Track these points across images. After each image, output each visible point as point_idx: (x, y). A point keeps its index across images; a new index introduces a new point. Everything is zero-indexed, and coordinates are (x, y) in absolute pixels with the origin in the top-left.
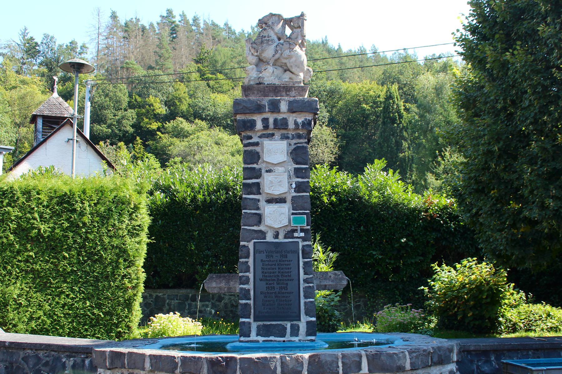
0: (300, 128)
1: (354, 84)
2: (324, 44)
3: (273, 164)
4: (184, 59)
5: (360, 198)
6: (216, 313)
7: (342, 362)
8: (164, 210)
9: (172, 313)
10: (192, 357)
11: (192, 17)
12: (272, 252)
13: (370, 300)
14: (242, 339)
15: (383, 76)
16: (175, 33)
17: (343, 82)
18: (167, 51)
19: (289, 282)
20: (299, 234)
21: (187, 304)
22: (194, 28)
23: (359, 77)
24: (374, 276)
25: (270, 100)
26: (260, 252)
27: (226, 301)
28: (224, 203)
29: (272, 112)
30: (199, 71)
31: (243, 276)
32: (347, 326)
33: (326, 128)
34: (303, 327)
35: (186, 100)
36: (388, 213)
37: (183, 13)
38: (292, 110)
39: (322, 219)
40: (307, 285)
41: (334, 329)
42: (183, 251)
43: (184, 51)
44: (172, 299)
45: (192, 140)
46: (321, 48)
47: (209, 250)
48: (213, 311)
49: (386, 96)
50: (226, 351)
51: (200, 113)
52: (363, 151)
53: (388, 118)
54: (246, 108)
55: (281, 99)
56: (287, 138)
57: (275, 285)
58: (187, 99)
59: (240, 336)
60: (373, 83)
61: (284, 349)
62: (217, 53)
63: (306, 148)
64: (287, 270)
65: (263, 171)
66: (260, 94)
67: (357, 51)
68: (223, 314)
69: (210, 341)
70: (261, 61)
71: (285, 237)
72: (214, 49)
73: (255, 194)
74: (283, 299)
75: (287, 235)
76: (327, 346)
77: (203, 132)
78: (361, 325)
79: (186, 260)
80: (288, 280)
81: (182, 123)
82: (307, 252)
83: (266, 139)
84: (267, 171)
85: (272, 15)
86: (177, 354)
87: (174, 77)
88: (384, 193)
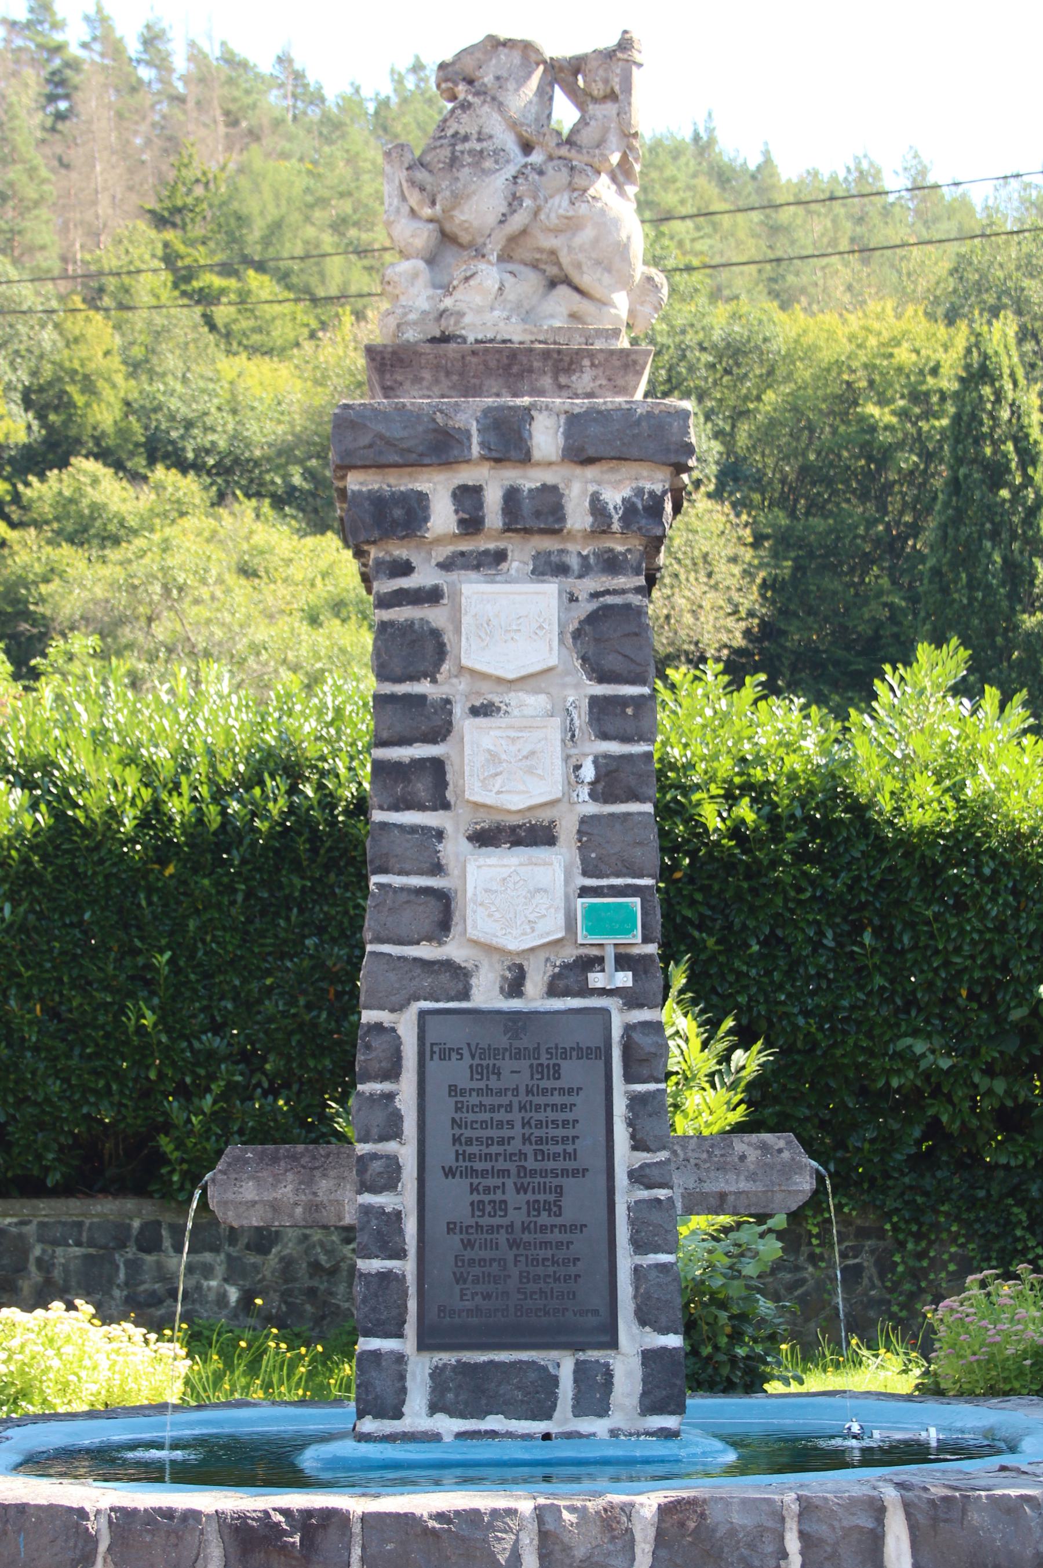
0: (616, 526)
1: (830, 319)
2: (702, 145)
3: (499, 680)
4: (104, 208)
5: (859, 809)
6: (247, 1300)
7: (802, 1535)
8: (26, 861)
9: (58, 1306)
10: (159, 1511)
11: (140, 29)
12: (495, 1052)
13: (902, 1245)
14: (368, 1425)
15: (952, 283)
16: (67, 97)
17: (784, 307)
18: (32, 171)
19: (568, 1183)
20: (611, 978)
21: (119, 1259)
22: (145, 73)
23: (849, 288)
24: (919, 1143)
25: (487, 411)
26: (445, 1054)
27: (289, 1247)
28: (282, 833)
29: (498, 459)
30: (169, 259)
31: (374, 1156)
32: (809, 1356)
33: (709, 504)
34: (629, 1374)
35: (114, 386)
36: (979, 874)
37: (99, 11)
38: (579, 454)
39: (699, 897)
40: (644, 1194)
41: (751, 1381)
42: (107, 1036)
43: (105, 175)
44: (55, 1243)
45: (138, 557)
46: (688, 158)
47: (215, 1034)
48: (233, 1295)
49: (968, 367)
50: (299, 1481)
51: (173, 442)
52: (866, 602)
53: (974, 461)
54: (390, 443)
55: (533, 405)
56: (561, 570)
57: (511, 1196)
58: (119, 379)
59: (361, 1415)
60: (910, 310)
61: (546, 1472)
62: (243, 182)
63: (639, 612)
64: (560, 1132)
65: (459, 710)
66: (445, 383)
67: (842, 175)
68: (277, 1306)
69: (227, 1430)
70: (448, 242)
71: (553, 991)
72: (232, 167)
73: (422, 808)
74: (542, 1253)
75: (561, 984)
76: (731, 1457)
77: (187, 523)
78: (865, 1352)
79: (118, 1075)
80: (565, 1173)
81: (95, 481)
82: (645, 1056)
83: (473, 575)
84: (475, 711)
85: (495, 44)
86: (95, 1497)
87: (63, 286)
88: (962, 785)
